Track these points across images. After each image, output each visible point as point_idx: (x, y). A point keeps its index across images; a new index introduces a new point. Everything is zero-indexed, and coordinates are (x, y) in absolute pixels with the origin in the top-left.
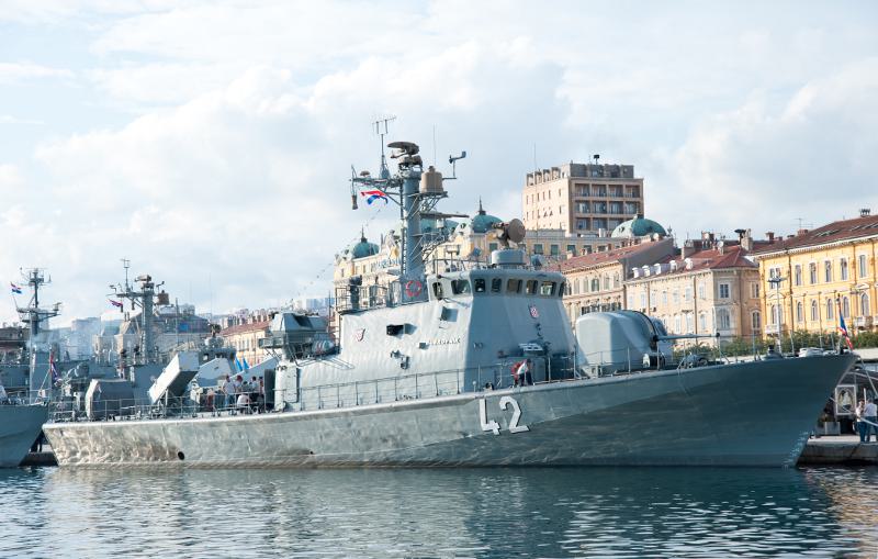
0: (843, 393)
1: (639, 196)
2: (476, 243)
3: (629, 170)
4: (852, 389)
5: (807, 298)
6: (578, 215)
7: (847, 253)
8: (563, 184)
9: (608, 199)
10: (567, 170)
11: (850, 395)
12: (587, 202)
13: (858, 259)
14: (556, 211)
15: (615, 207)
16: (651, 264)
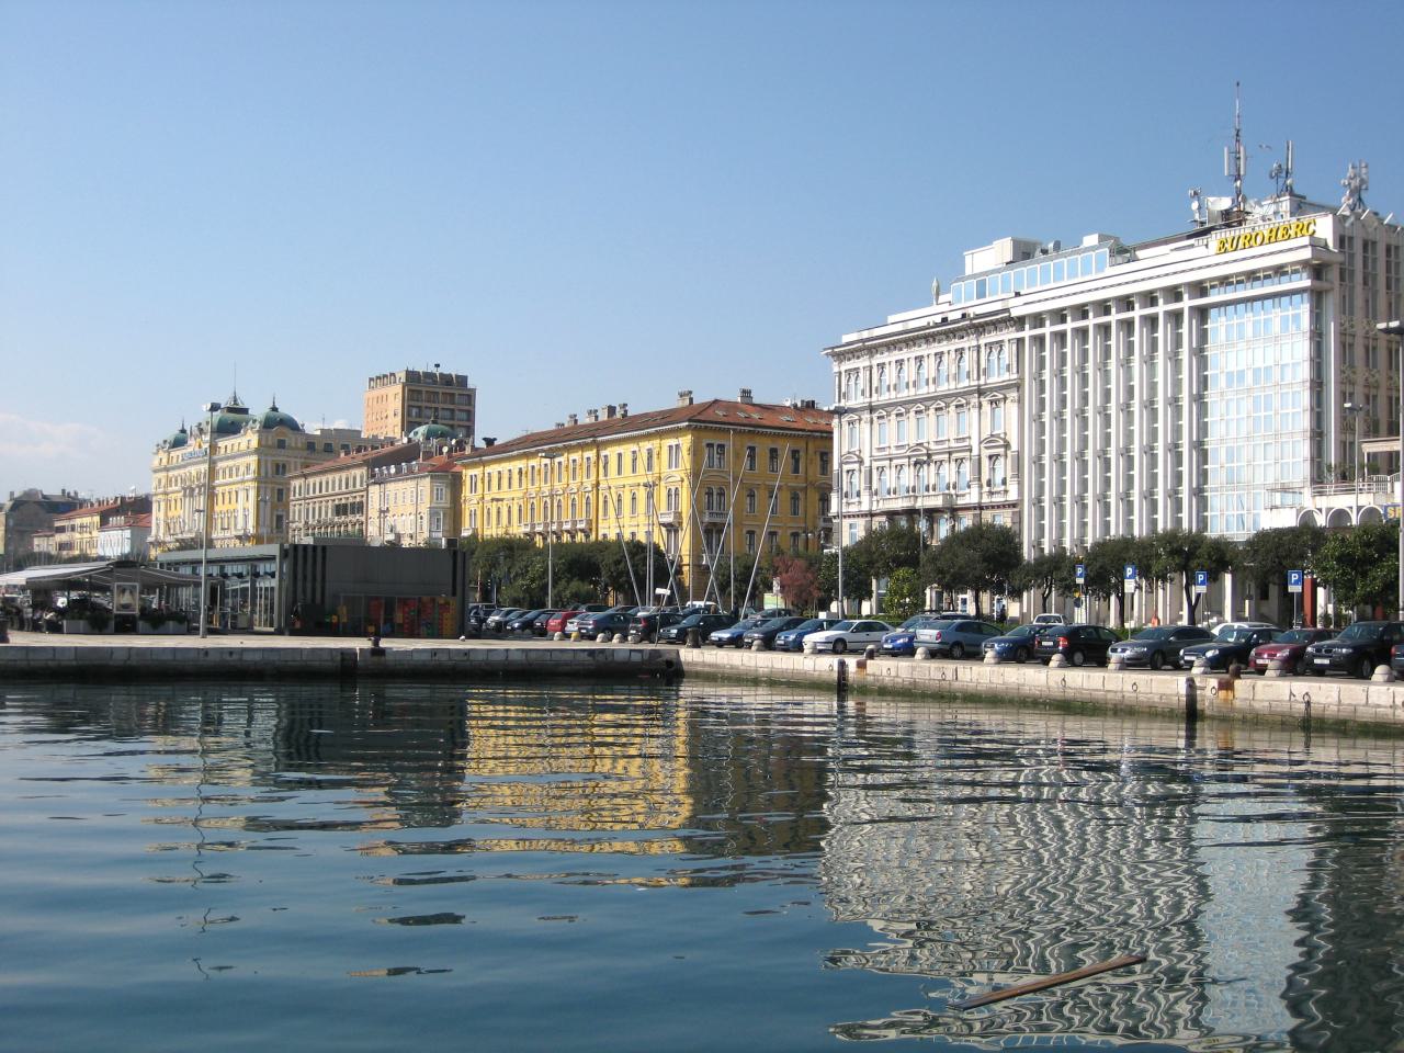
0: (123, 591)
1: (470, 404)
2: (264, 438)
3: (463, 380)
4: (134, 587)
5: (515, 502)
6: (411, 419)
7: (521, 464)
8: (398, 389)
9: (440, 406)
10: (402, 376)
11: (131, 592)
12: (419, 407)
13: (530, 469)
14: (391, 414)
15: (464, 416)
16: (397, 464)
